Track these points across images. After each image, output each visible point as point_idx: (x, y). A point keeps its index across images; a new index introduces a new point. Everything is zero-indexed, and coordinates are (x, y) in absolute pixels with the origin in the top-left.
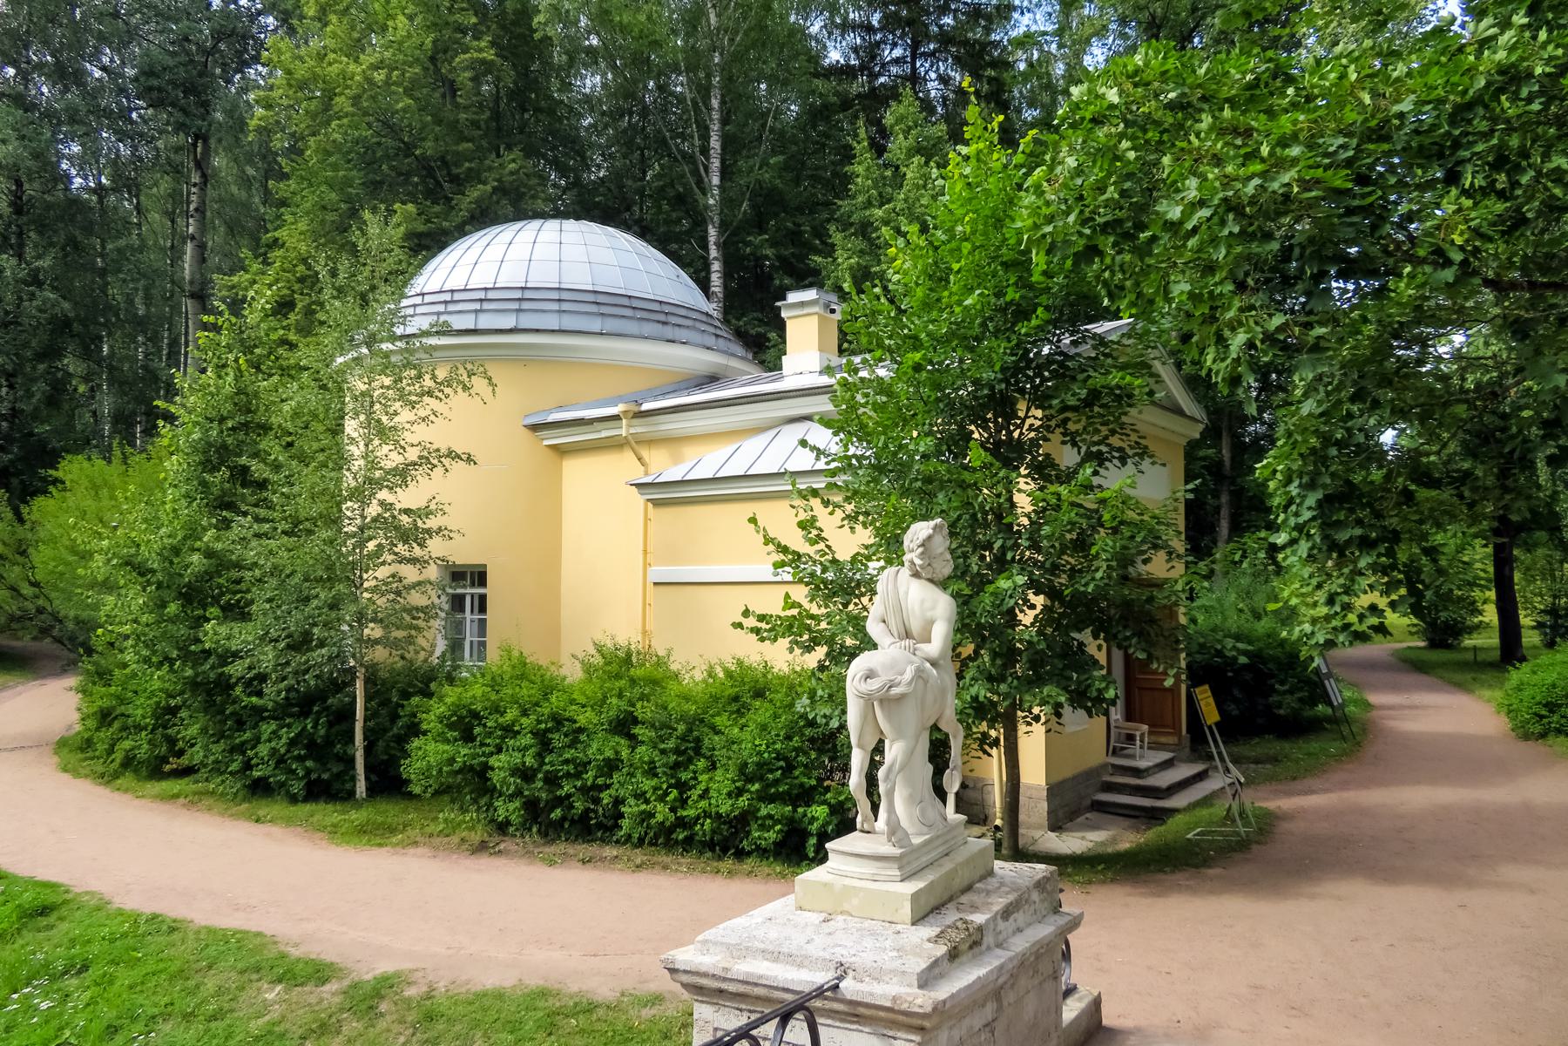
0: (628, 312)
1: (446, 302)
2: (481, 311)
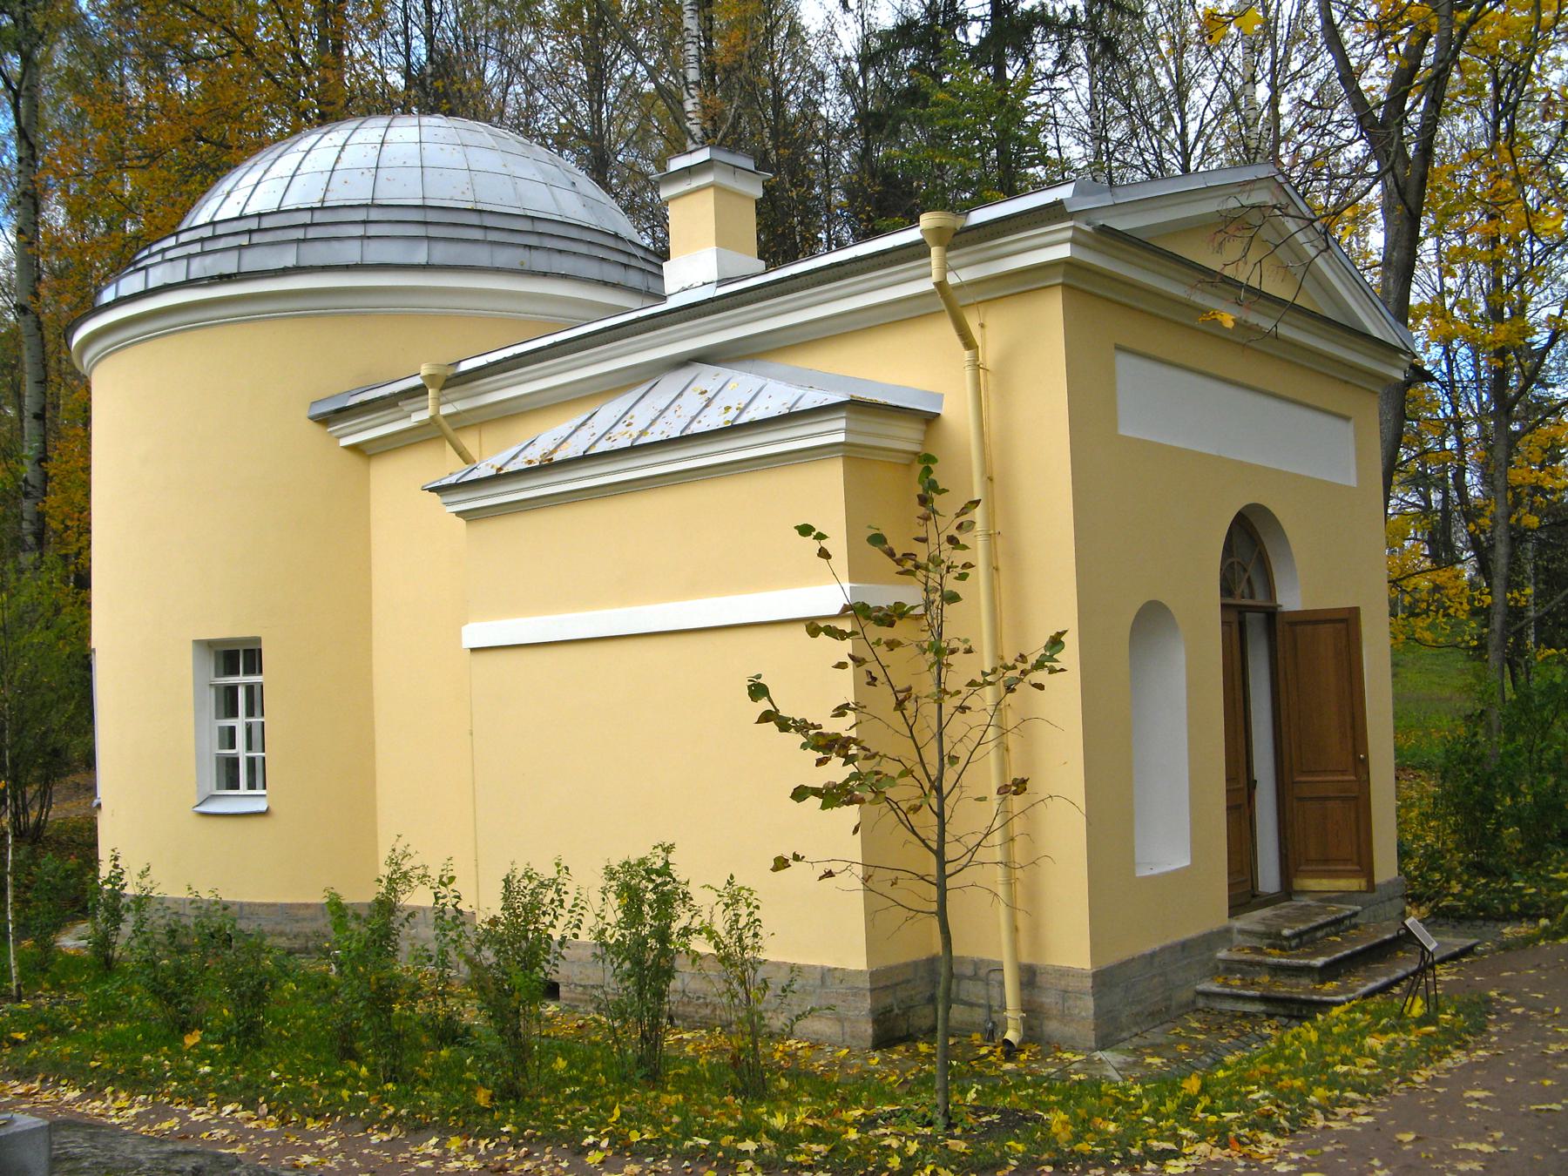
0: (477, 234)
1: (250, 232)
2: (250, 246)
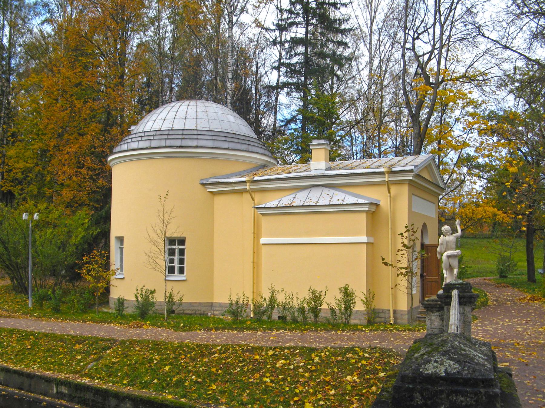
0: (224, 139)
